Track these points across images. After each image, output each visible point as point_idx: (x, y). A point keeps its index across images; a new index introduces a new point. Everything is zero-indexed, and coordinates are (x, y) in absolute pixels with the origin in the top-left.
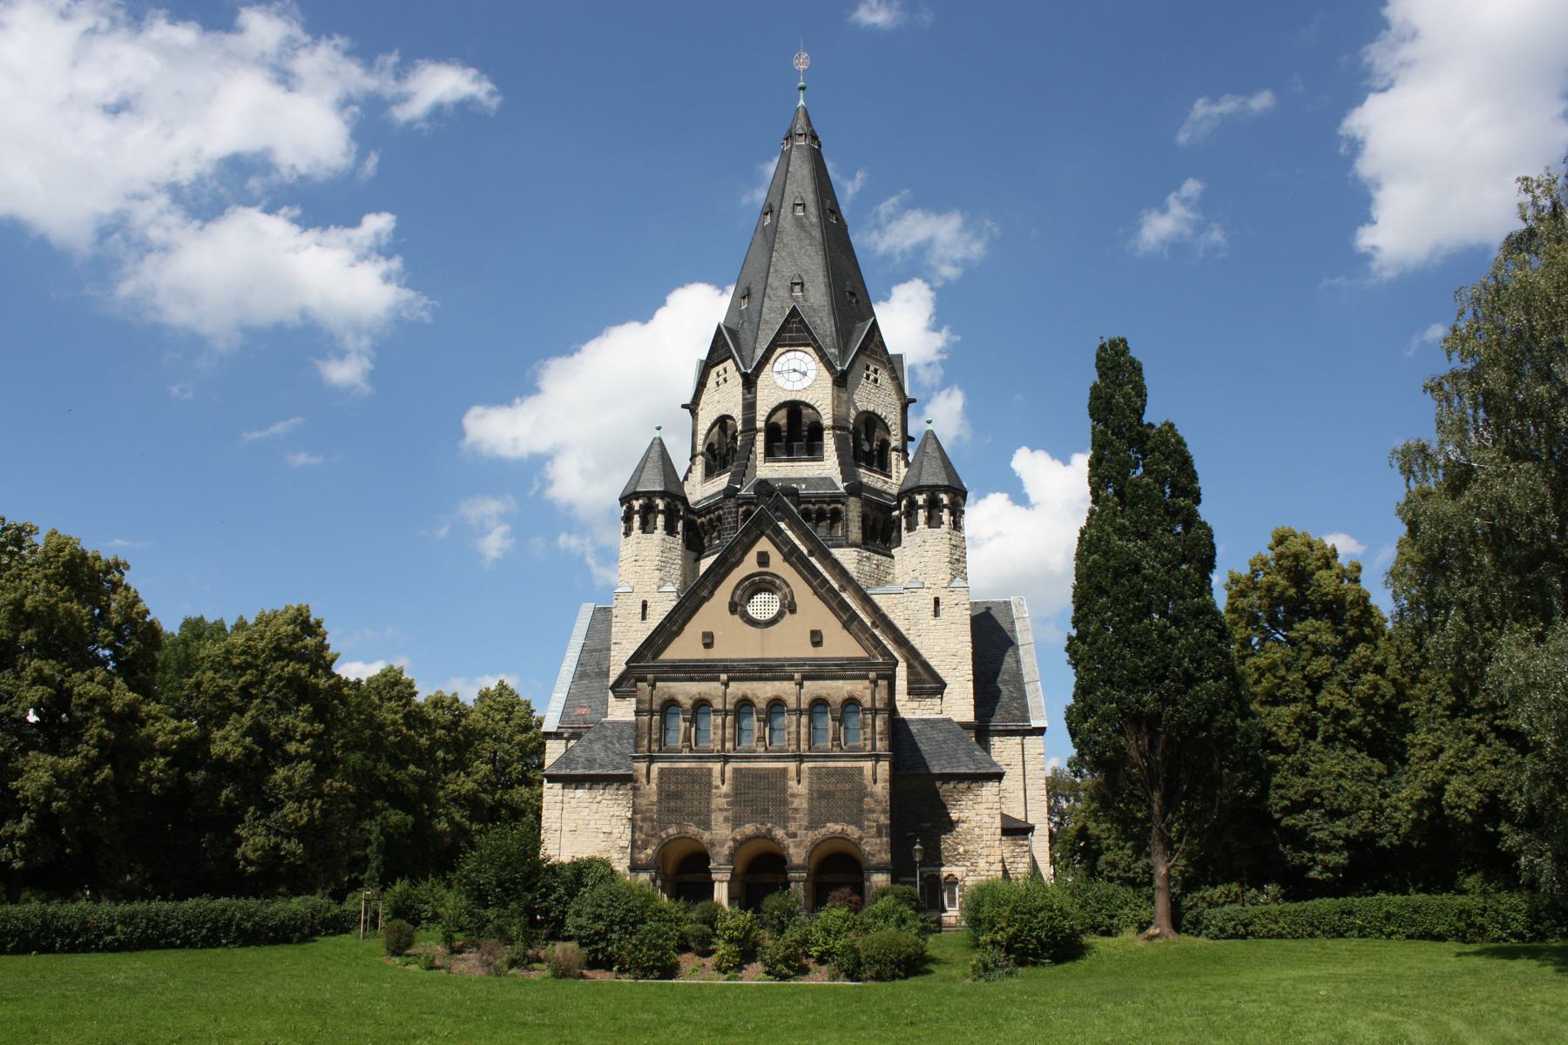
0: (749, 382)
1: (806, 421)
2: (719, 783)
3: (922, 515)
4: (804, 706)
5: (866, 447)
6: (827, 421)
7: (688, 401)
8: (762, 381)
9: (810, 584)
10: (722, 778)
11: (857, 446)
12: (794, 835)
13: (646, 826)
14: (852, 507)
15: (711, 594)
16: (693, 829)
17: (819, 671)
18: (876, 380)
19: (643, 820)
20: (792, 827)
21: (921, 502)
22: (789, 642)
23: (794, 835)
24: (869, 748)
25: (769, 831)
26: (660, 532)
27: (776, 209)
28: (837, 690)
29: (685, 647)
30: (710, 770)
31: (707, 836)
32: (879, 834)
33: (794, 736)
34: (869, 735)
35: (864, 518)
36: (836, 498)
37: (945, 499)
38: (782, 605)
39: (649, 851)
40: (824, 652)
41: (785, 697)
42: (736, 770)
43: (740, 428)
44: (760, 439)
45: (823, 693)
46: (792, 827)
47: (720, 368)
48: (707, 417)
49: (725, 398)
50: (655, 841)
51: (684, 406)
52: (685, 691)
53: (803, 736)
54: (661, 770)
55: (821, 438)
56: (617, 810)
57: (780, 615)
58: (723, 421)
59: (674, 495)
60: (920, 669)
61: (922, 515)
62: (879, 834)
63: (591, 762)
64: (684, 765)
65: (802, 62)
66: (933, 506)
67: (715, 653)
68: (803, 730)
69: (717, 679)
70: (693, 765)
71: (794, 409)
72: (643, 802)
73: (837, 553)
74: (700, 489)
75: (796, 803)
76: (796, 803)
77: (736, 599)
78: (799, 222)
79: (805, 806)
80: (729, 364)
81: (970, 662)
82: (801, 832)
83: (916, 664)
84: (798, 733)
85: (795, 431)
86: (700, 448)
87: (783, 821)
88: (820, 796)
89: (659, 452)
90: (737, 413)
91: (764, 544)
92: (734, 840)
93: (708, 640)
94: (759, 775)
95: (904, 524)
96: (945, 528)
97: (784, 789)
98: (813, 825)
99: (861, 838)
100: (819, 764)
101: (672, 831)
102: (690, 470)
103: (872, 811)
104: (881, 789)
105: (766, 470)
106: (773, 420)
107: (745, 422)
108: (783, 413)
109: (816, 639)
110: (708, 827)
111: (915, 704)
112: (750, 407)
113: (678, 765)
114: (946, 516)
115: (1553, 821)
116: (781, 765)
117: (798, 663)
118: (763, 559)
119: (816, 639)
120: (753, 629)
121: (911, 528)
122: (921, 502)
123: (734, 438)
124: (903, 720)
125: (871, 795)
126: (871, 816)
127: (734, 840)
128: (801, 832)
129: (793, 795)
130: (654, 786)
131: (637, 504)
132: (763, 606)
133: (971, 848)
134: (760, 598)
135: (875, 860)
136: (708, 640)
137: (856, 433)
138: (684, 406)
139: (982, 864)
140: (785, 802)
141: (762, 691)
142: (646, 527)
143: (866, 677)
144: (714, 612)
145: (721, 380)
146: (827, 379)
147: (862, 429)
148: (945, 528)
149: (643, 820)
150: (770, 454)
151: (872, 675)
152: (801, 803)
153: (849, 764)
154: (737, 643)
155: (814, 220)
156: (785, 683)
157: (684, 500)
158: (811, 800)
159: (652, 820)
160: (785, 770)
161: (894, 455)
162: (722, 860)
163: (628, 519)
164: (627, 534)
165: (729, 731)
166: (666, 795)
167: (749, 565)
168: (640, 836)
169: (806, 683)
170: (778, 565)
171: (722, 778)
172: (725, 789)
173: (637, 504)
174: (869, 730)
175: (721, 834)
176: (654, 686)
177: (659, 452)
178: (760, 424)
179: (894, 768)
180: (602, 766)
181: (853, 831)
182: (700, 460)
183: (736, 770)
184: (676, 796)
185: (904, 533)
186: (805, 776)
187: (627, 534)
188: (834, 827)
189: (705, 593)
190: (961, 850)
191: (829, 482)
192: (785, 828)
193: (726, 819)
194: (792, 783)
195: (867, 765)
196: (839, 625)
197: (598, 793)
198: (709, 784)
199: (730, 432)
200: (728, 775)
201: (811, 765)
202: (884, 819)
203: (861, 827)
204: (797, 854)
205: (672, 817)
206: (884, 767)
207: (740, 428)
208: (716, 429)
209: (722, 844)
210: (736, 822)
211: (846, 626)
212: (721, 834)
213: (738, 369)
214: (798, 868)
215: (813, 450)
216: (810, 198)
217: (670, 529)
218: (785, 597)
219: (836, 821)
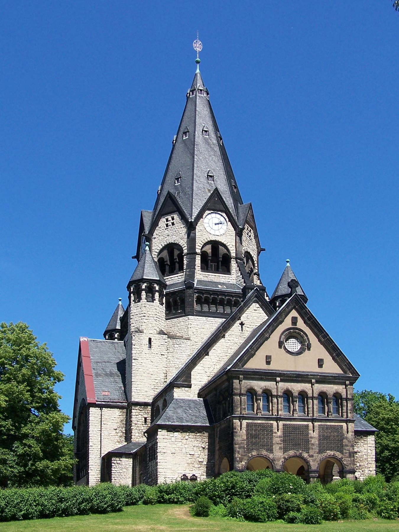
4: (315, 395)
10: (278, 430)
12: (312, 456)
16: (264, 453)
17: (323, 379)
19: (240, 448)
22: (307, 363)
23: (312, 456)
24: (345, 416)
25: (301, 454)
26: (157, 302)
28: (331, 389)
29: (256, 363)
31: (271, 456)
39: (243, 463)
41: (307, 390)
46: (311, 453)
52: (259, 385)
56: (196, 443)
63: (181, 419)
64: (259, 422)
65: (198, 46)
70: (264, 422)
71: (215, 245)
76: (313, 441)
77: (282, 340)
78: (206, 141)
79: (317, 443)
82: (316, 455)
87: (307, 450)
90: (183, 243)
92: (284, 458)
94: (295, 427)
97: (308, 434)
98: (320, 452)
99: (342, 458)
100: (323, 423)
101: (254, 453)
103: (347, 446)
105: (201, 277)
106: (204, 249)
107: (188, 249)
109: (320, 363)
112: (192, 240)
113: (256, 421)
117: (314, 375)
119: (320, 363)
125: (346, 438)
127: (284, 458)
128: (316, 455)
129: (311, 438)
130: (244, 431)
133: (362, 464)
134: (293, 340)
139: (367, 471)
141: (296, 387)
144: (270, 346)
145: (170, 223)
153: (337, 424)
154: (282, 363)
158: (319, 440)
159: (244, 448)
160: (307, 426)
167: (287, 323)
171: (278, 430)
172: (279, 433)
178: (198, 251)
180: (187, 421)
181: (338, 455)
184: (256, 436)
186: (316, 428)
189: (267, 335)
190: (358, 465)
193: (280, 448)
194: (311, 432)
197: (186, 435)
200: (281, 427)
201: (319, 423)
203: (342, 452)
205: (254, 447)
207: (185, 251)
209: (279, 460)
210: (285, 450)
214: (314, 472)
215: (227, 271)
216: (210, 128)
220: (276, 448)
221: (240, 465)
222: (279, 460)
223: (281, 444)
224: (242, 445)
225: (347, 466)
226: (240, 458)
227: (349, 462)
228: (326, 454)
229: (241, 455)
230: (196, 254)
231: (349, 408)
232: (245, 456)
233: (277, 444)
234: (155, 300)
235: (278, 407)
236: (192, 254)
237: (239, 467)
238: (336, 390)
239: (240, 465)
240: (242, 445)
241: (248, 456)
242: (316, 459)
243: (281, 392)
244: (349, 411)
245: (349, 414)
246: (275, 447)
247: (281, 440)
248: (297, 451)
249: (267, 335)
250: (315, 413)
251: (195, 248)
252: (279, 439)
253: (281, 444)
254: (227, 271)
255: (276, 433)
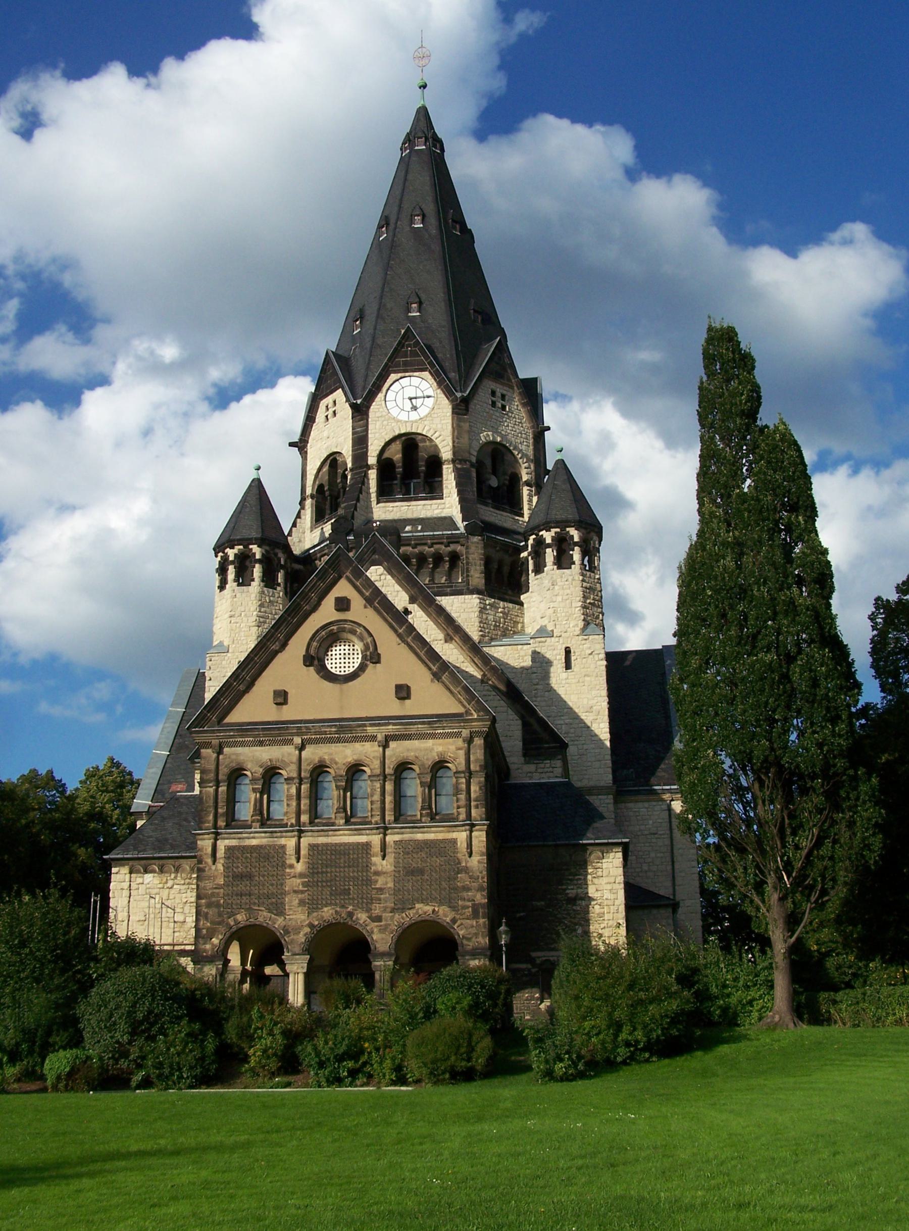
0: (360, 412)
1: (423, 454)
2: (293, 861)
3: (550, 555)
5: (494, 482)
6: (446, 453)
7: (296, 439)
8: (375, 409)
9: (396, 631)
11: (481, 481)
12: (378, 919)
13: (212, 912)
14: (473, 549)
15: (284, 645)
16: (264, 917)
18: (503, 408)
19: (209, 905)
20: (377, 910)
21: (549, 540)
22: (372, 697)
23: (378, 919)
24: (463, 816)
26: (256, 585)
27: (392, 221)
29: (254, 707)
30: (283, 847)
32: (475, 915)
33: (377, 805)
34: (463, 802)
35: (487, 562)
36: (454, 539)
37: (575, 534)
38: (364, 657)
39: (215, 941)
40: (410, 708)
42: (312, 847)
43: (349, 465)
44: (373, 475)
45: (411, 756)
46: (377, 910)
47: (329, 400)
48: (317, 454)
49: (334, 434)
50: (222, 929)
51: (291, 444)
52: (254, 756)
53: (389, 805)
54: (229, 849)
55: (440, 475)
57: (362, 668)
58: (333, 460)
59: (274, 538)
60: (536, 726)
61: (550, 555)
62: (475, 915)
66: (562, 544)
67: (288, 713)
68: (389, 799)
69: (290, 742)
71: (410, 442)
72: (208, 884)
73: (447, 602)
74: (307, 537)
75: (380, 882)
76: (380, 882)
77: (312, 652)
80: (339, 395)
81: (606, 718)
83: (532, 721)
84: (383, 802)
85: (410, 466)
86: (309, 491)
87: (366, 903)
88: (408, 872)
89: (257, 498)
91: (343, 589)
92: (311, 926)
93: (281, 698)
95: (531, 567)
96: (576, 568)
97: (367, 866)
98: (401, 906)
99: (454, 921)
102: (299, 516)
103: (467, 889)
104: (477, 862)
106: (386, 455)
107: (355, 458)
108: (397, 447)
109: (403, 692)
110: (281, 912)
111: (532, 767)
112: (360, 441)
114: (576, 554)
115: (123, 1014)
116: (363, 839)
118: (343, 604)
119: (403, 692)
120: (330, 685)
121: (539, 570)
122: (549, 540)
123: (345, 477)
124: (579, 789)
125: (466, 870)
126: (465, 894)
127: (311, 926)
129: (377, 873)
130: (220, 867)
131: (231, 553)
132: (343, 659)
135: (470, 945)
136: (281, 698)
137: (479, 466)
138: (291, 444)
140: (368, 882)
141: (343, 754)
142: (243, 579)
143: (458, 735)
144: (288, 667)
146: (446, 407)
147: (488, 462)
148: (576, 568)
149: (209, 905)
150: (385, 493)
151: (465, 733)
152: (385, 882)
153: (440, 836)
154: (312, 700)
155: (434, 232)
156: (368, 745)
157: (287, 548)
159: (218, 905)
160: (367, 846)
161: (525, 491)
162: (297, 950)
163: (222, 570)
164: (222, 587)
165: (305, 803)
166: (235, 877)
167: (326, 613)
168: (205, 924)
169: (393, 744)
170: (360, 612)
172: (300, 867)
173: (231, 553)
174: (462, 797)
175: (296, 920)
176: (220, 752)
177: (257, 498)
178: (372, 460)
179: (494, 835)
181: (445, 914)
182: (309, 502)
183: (312, 847)
185: (532, 575)
187: (222, 587)
188: (424, 909)
189: (276, 647)
191: (448, 522)
192: (369, 910)
193: (302, 903)
194: (376, 859)
195: (461, 836)
196: (428, 676)
198: (284, 865)
199: (340, 471)
202: (481, 898)
203: (454, 908)
204: (381, 939)
206: (480, 837)
207: (349, 465)
208: (326, 469)
209: (297, 930)
210: (312, 905)
211: (436, 676)
212: (296, 920)
213: (348, 400)
214: (383, 955)
215: (433, 490)
217: (269, 580)
218: (366, 647)
219: (424, 901)
220: (292, 902)
221: (208, 946)
222: (297, 930)
223: (302, 892)
224: (214, 899)
225: (469, 939)
226: (208, 929)
227: (474, 931)
228: (412, 912)
229: (212, 923)
230: (369, 467)
231: (473, 795)
232: (219, 923)
233: (295, 892)
234: (253, 580)
235: (299, 805)
236: (361, 467)
237: (205, 951)
238: (440, 754)
239: (208, 946)
240: (214, 899)
241: (228, 924)
242: (387, 926)
243: (389, 768)
244: (473, 804)
245: (473, 811)
246: (291, 901)
247: (303, 884)
248: (343, 906)
249: (276, 647)
250: (387, 813)
251: (365, 455)
252: (299, 881)
253: (302, 892)
254: (433, 490)
255: (291, 866)
